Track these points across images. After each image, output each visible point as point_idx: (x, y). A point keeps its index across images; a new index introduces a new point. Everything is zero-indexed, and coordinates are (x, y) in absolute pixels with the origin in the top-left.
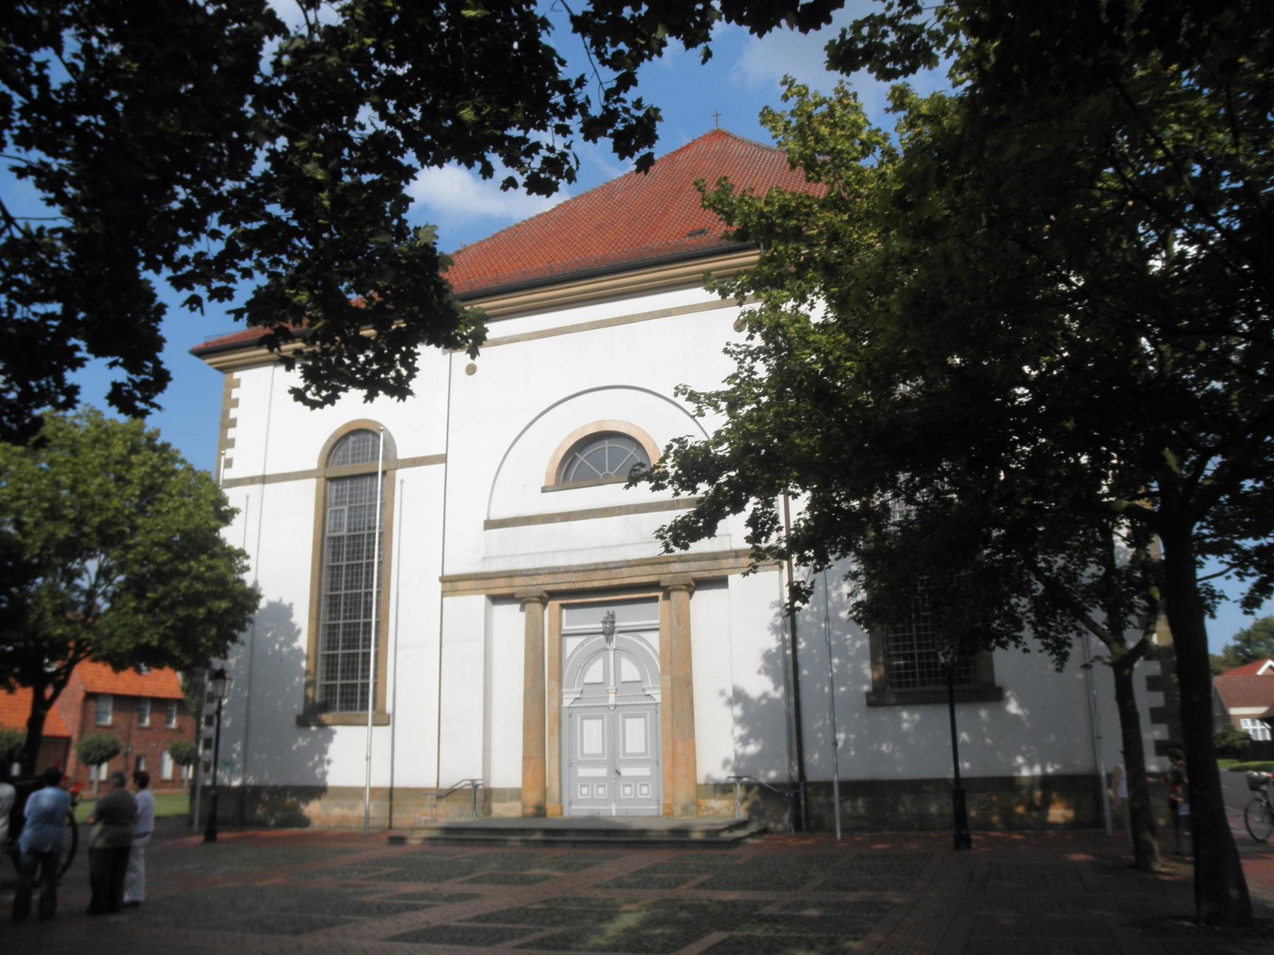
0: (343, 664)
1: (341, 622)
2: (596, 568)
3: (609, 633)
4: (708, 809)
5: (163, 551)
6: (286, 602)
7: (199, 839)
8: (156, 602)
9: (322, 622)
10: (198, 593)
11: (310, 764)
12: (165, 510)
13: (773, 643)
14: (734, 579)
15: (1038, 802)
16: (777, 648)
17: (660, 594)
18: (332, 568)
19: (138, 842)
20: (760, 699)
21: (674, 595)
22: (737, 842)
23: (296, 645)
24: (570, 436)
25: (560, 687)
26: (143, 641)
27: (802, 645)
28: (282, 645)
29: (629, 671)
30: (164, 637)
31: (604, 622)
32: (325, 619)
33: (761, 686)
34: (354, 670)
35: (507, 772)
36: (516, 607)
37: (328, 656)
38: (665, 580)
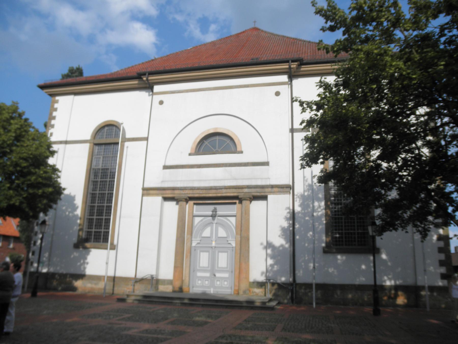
0: (96, 222)
1: (96, 205)
2: (211, 188)
3: (214, 216)
4: (253, 292)
5: (24, 162)
6: (72, 194)
7: (29, 295)
8: (18, 186)
9: (88, 204)
10: (39, 183)
11: (79, 264)
12: (25, 145)
13: (285, 224)
14: (270, 197)
15: (392, 296)
16: (288, 227)
17: (237, 201)
18: (94, 182)
19: (14, 300)
20: (279, 247)
21: (244, 202)
22: (272, 308)
23: (76, 213)
24: (202, 133)
25: (192, 238)
26: (12, 202)
27: (297, 226)
28: (69, 212)
29: (222, 233)
30: (21, 203)
31: (213, 212)
32: (89, 203)
33: (279, 241)
34: (101, 226)
35: (167, 272)
36: (174, 203)
37: (89, 219)
38: (241, 196)
